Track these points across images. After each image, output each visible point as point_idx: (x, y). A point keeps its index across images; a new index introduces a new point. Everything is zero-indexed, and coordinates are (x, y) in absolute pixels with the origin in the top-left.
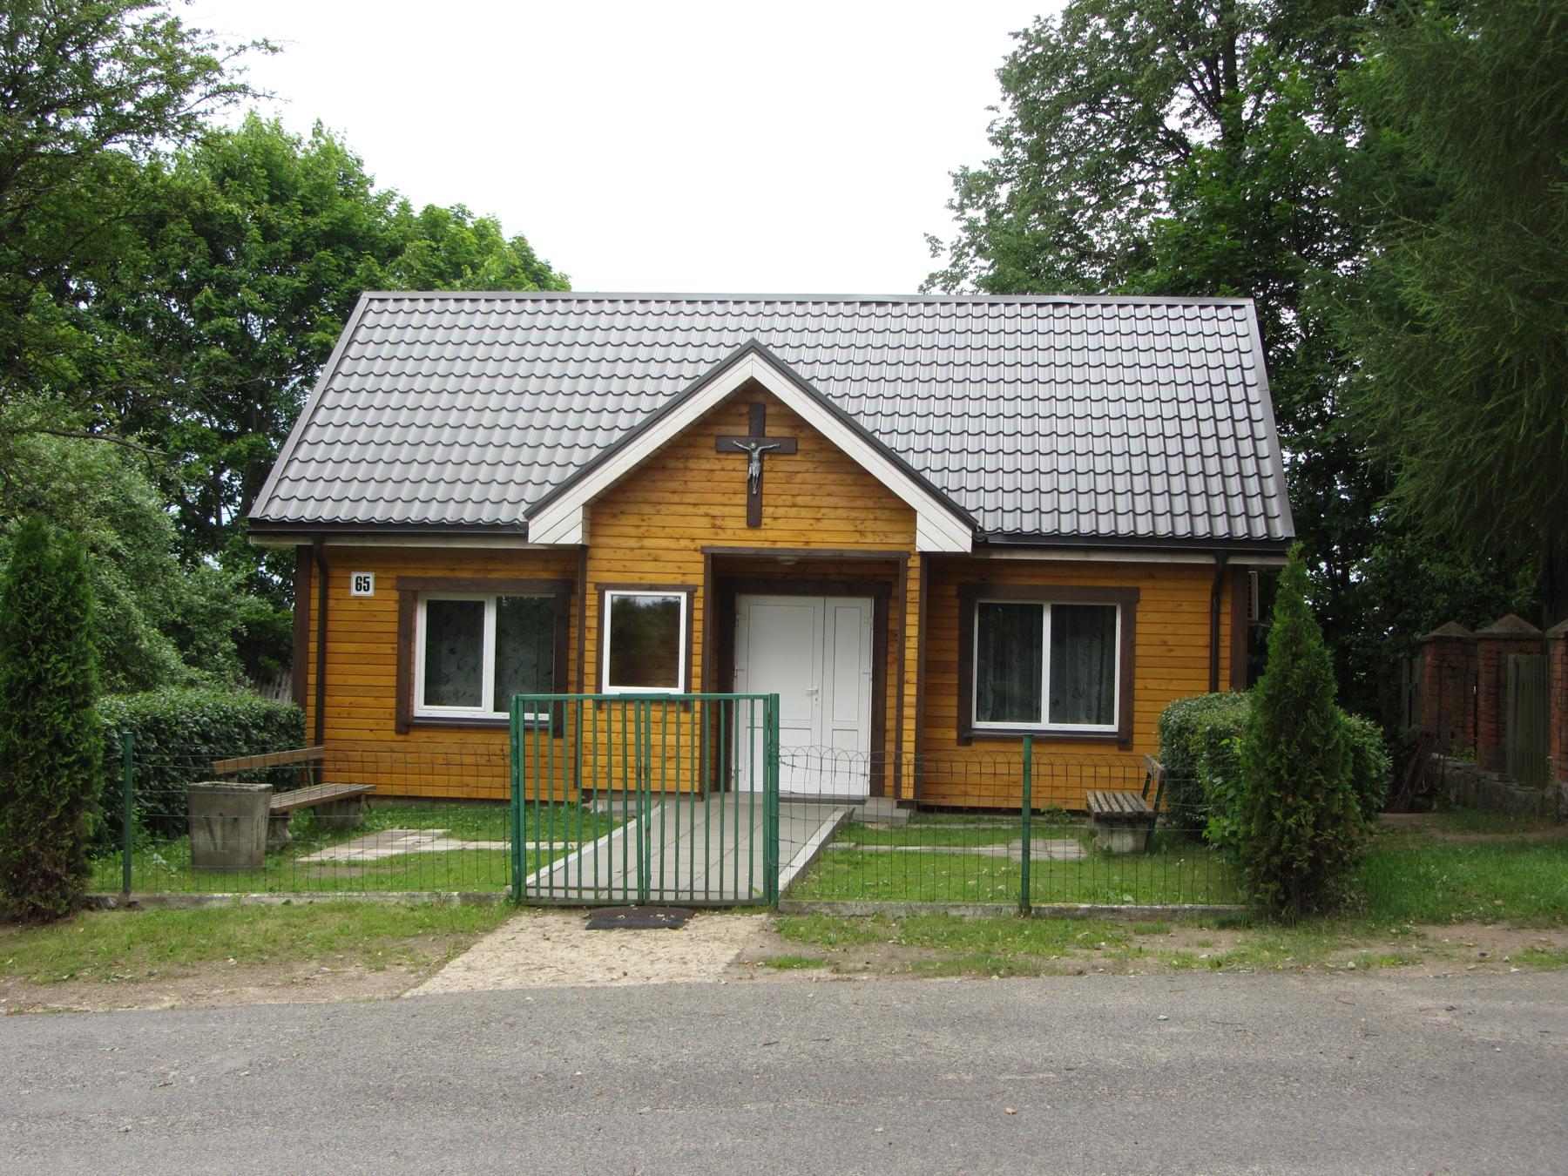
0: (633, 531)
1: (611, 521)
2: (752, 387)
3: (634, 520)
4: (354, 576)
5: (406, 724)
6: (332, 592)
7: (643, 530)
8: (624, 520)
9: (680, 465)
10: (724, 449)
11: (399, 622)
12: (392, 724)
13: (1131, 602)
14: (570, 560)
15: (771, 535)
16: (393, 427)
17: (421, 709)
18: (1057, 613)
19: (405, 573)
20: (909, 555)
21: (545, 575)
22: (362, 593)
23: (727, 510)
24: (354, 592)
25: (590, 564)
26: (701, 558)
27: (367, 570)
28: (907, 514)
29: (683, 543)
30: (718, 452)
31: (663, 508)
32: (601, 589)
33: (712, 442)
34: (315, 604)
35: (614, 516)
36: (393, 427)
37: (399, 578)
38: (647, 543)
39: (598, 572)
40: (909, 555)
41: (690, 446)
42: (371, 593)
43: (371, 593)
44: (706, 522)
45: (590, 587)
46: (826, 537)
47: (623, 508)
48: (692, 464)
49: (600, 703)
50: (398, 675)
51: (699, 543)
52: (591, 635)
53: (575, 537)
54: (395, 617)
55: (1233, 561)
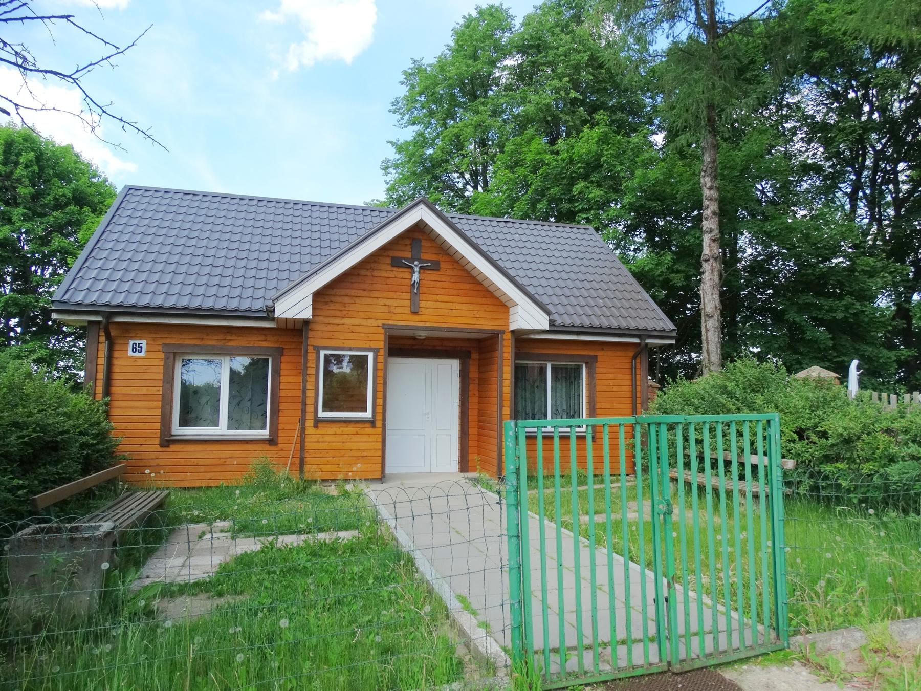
0: (338, 313)
1: (324, 307)
2: (420, 228)
3: (338, 306)
4: (131, 342)
5: (168, 441)
6: (117, 347)
7: (344, 312)
8: (332, 306)
9: (369, 273)
10: (397, 263)
11: (164, 374)
12: (157, 441)
13: (591, 362)
14: (296, 332)
15: (424, 318)
16: (94, 277)
17: (178, 430)
18: (554, 369)
19: (168, 341)
20: (504, 332)
21: (264, 344)
22: (137, 354)
23: (398, 302)
24: (131, 353)
25: (311, 334)
26: (382, 331)
27: (141, 338)
28: (502, 305)
29: (370, 322)
30: (393, 266)
31: (358, 301)
32: (318, 349)
33: (389, 261)
34: (102, 361)
35: (327, 303)
36: (94, 277)
37: (165, 345)
38: (346, 321)
39: (314, 339)
40: (504, 332)
41: (375, 262)
42: (143, 354)
43: (143, 354)
44: (385, 309)
45: (310, 349)
46: (459, 320)
47: (332, 298)
48: (376, 273)
49: (318, 422)
50: (163, 408)
51: (380, 323)
52: (311, 379)
53: (307, 314)
54: (161, 370)
55: (649, 341)
